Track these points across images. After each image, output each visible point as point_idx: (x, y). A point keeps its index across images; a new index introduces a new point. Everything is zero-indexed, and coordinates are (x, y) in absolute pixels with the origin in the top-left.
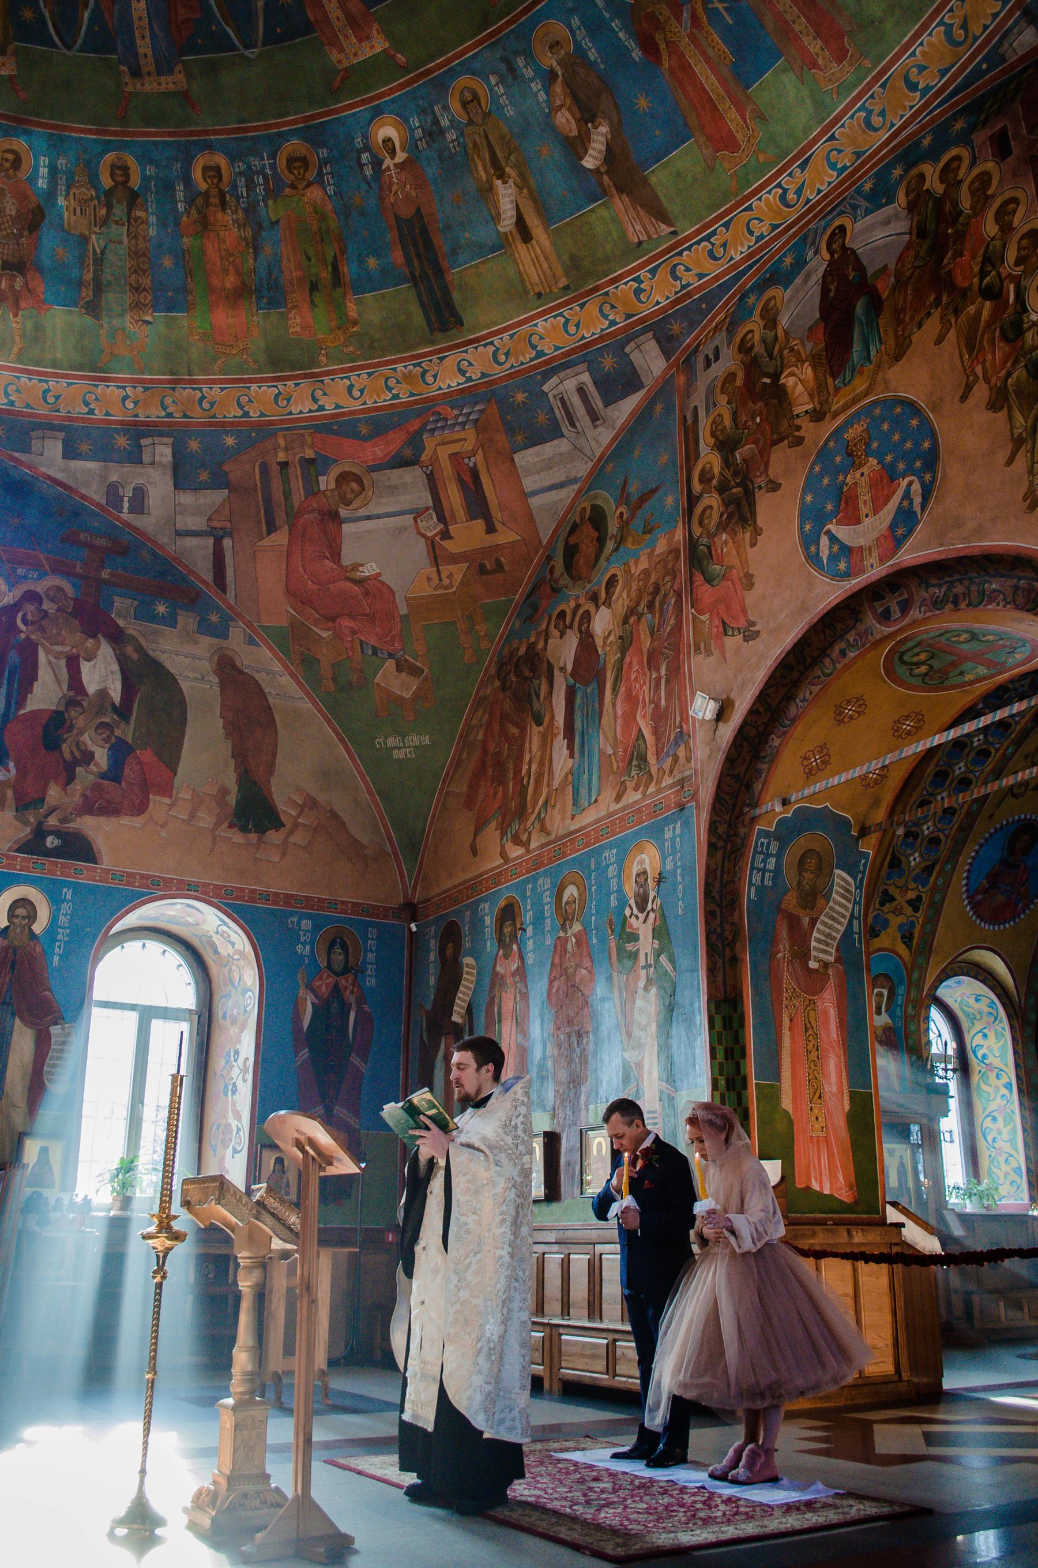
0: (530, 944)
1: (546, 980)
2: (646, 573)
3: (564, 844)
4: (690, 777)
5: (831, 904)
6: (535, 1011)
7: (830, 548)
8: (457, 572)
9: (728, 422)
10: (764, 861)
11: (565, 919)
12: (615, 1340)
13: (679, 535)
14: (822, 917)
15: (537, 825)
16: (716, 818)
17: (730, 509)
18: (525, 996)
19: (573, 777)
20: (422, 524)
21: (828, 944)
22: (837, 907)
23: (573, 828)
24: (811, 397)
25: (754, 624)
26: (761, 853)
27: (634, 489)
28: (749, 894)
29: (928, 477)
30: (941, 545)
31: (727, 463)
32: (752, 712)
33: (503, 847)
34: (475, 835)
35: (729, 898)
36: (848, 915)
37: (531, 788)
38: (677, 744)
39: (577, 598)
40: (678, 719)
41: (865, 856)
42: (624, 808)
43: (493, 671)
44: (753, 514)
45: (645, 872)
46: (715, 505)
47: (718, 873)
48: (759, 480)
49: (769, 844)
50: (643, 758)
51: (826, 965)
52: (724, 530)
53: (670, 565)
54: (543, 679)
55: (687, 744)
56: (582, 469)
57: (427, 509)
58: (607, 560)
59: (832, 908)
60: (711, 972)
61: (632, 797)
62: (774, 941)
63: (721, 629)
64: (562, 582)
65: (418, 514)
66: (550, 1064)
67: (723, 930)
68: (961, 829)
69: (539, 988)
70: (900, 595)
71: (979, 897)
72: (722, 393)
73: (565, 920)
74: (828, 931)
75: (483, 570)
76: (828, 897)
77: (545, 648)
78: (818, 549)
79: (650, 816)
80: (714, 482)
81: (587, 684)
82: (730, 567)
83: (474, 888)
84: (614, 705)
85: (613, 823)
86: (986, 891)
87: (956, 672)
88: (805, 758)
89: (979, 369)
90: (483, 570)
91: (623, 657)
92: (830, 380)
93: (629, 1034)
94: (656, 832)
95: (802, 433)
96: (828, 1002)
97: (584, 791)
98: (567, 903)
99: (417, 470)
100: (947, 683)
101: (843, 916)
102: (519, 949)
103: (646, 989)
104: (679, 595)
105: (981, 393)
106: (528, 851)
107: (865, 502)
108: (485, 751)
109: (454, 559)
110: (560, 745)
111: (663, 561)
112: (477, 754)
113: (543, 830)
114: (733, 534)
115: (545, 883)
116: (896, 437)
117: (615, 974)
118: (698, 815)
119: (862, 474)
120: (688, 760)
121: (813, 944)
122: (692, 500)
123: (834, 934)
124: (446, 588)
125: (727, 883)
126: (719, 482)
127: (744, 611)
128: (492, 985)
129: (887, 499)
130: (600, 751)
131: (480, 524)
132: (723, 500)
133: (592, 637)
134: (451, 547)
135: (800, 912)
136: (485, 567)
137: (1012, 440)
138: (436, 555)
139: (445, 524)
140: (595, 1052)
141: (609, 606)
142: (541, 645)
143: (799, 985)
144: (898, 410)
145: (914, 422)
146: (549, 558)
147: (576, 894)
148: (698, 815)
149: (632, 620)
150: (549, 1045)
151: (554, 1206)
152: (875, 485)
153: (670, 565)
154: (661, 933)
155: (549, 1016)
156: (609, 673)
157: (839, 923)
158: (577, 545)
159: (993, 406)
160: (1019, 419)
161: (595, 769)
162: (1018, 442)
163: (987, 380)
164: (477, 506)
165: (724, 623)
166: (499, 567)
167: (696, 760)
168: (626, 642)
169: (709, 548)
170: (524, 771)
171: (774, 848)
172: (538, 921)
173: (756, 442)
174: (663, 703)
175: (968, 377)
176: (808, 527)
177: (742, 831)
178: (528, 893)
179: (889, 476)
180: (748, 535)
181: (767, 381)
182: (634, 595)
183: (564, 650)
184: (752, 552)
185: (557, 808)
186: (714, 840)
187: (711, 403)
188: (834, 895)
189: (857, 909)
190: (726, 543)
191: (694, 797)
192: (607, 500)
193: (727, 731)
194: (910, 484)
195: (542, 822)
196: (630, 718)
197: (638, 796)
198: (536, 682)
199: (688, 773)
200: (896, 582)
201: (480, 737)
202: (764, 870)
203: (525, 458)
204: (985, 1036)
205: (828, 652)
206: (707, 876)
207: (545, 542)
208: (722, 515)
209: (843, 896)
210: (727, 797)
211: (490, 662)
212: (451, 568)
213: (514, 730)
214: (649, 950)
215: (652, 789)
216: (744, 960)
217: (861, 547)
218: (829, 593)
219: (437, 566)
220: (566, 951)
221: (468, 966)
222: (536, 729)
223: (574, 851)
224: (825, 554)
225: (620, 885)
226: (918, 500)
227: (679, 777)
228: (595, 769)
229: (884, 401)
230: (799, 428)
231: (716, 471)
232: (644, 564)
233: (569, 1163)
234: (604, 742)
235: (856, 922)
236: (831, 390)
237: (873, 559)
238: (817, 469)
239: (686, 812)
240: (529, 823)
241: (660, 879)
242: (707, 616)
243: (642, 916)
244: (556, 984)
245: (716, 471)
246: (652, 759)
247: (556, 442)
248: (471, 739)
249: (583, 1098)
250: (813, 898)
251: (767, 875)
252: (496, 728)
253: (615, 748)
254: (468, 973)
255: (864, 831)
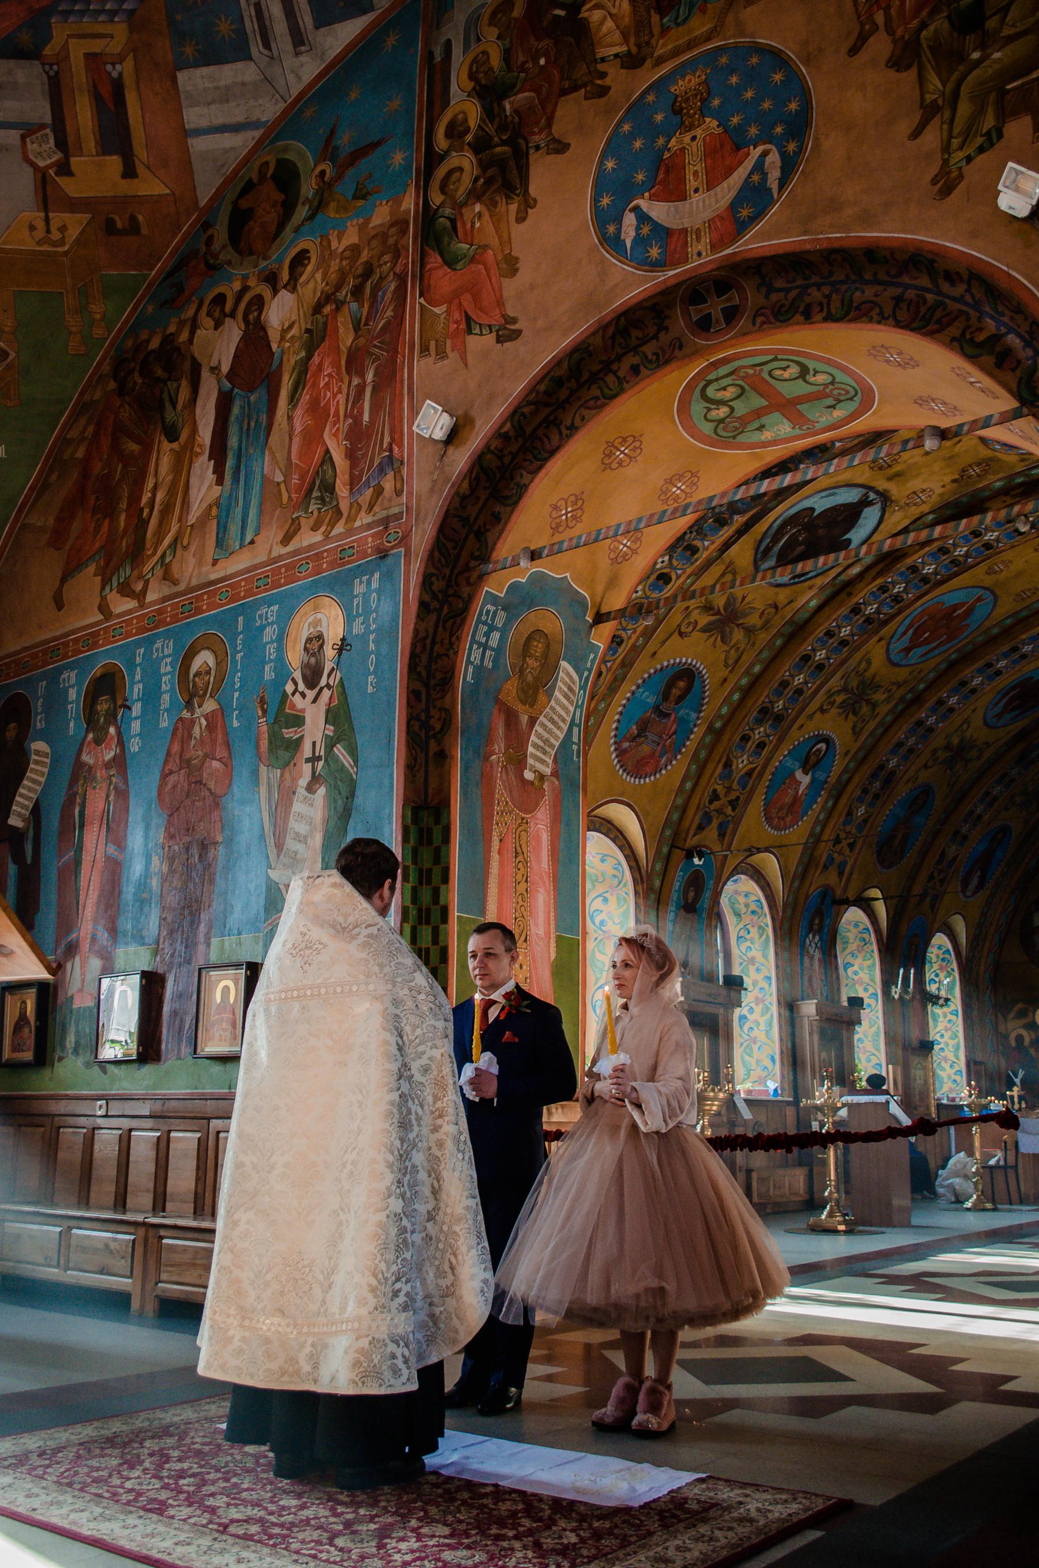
0: (136, 726)
1: (157, 776)
2: (355, 250)
3: (199, 598)
4: (398, 516)
5: (553, 703)
6: (136, 813)
7: (638, 229)
8: (75, 224)
9: (496, 61)
10: (487, 635)
11: (192, 696)
12: (70, 1228)
13: (409, 203)
14: (542, 718)
15: (159, 572)
16: (433, 570)
17: (490, 173)
18: (123, 795)
19: (220, 512)
20: (32, 147)
21: (545, 753)
22: (558, 708)
23: (213, 577)
24: (625, 35)
25: (514, 320)
26: (485, 623)
27: (345, 141)
28: (465, 675)
29: (792, 147)
30: (805, 233)
31: (489, 113)
32: (499, 435)
33: (103, 598)
34: (63, 580)
35: (439, 675)
36: (569, 719)
37: (153, 522)
38: (381, 470)
39: (245, 278)
40: (387, 440)
41: (594, 649)
42: (295, 553)
43: (106, 368)
44: (525, 180)
45: (320, 637)
46: (466, 165)
47: (428, 642)
48: (536, 138)
49: (495, 613)
50: (329, 488)
51: (542, 777)
52: (479, 199)
53: (391, 241)
54: (184, 383)
55: (398, 472)
56: (269, 110)
57: (43, 126)
58: (297, 230)
59: (553, 709)
60: (411, 769)
61: (308, 538)
62: (490, 740)
63: (463, 326)
64: (223, 257)
65: (29, 131)
66: (155, 883)
67: (429, 717)
68: (623, 664)
69: (145, 784)
70: (730, 299)
71: (626, 745)
72: (490, 24)
73: (191, 693)
74: (546, 735)
75: (110, 228)
76: (550, 695)
77: (191, 340)
78: (619, 230)
79: (333, 565)
80: (469, 138)
81: (251, 390)
82: (485, 247)
83: (56, 651)
84: (290, 418)
85: (276, 572)
86: (634, 739)
87: (756, 424)
88: (556, 508)
89: (879, 18)
90: (110, 228)
91: (309, 357)
92: (655, 18)
93: (279, 847)
94: (340, 587)
95: (608, 81)
96: (541, 823)
97: (234, 529)
98: (198, 674)
99: (35, 68)
100: (740, 439)
101: (564, 720)
102: (119, 733)
103: (310, 789)
104: (402, 279)
105: (880, 46)
106: (142, 605)
107: (696, 173)
108: (85, 474)
109: (74, 205)
110: (203, 470)
111: (383, 236)
112: (75, 475)
113: (167, 576)
114: (492, 204)
115: (166, 650)
116: (749, 94)
117: (263, 769)
118: (408, 564)
119: (694, 138)
120: (398, 493)
121: (530, 749)
122: (432, 159)
123: (552, 740)
124: (55, 244)
125: (439, 656)
126: (476, 137)
127: (500, 303)
128: (74, 780)
129: (729, 172)
130: (263, 476)
131: (114, 162)
132: (480, 162)
133: (264, 329)
134: (70, 187)
135: (519, 707)
136: (114, 222)
137: (922, 106)
138: (47, 195)
139: (67, 156)
140: (227, 869)
141: (293, 290)
142: (184, 336)
143: (512, 797)
144: (754, 60)
145: (778, 77)
146: (206, 225)
147: (211, 662)
148: (408, 564)
149: (327, 309)
150: (156, 861)
151: (148, 1069)
152: (712, 152)
153: (391, 241)
154: (339, 716)
155: (159, 820)
156: (286, 377)
157: (559, 728)
158: (251, 210)
159: (897, 63)
160: (934, 81)
161: (254, 502)
162: (929, 112)
163: (890, 30)
164: (115, 137)
165: (468, 319)
166: (133, 227)
167: (410, 494)
168: (315, 338)
169: (453, 221)
170: (144, 500)
171: (500, 620)
172: (151, 697)
173: (537, 90)
174: (366, 417)
175: (862, 25)
176: (605, 201)
177: (465, 591)
178: (138, 660)
179: (729, 147)
180: (513, 207)
181: (561, 13)
182: (333, 277)
183: (221, 345)
184: (518, 231)
185: (192, 548)
186: (427, 598)
187: (472, 32)
188: (557, 693)
189: (578, 714)
190: (480, 215)
191: (404, 540)
192: (302, 154)
193: (461, 459)
194: (765, 154)
195: (167, 569)
196: (313, 437)
197: (318, 537)
198: (172, 385)
199: (395, 510)
200: (724, 280)
201: (80, 454)
202: (485, 647)
203: (193, 80)
204: (606, 900)
205: (614, 367)
206: (414, 645)
207: (202, 203)
208: (476, 180)
209: (566, 696)
210: (449, 545)
211: (107, 353)
212: (66, 216)
213: (133, 447)
214: (319, 738)
215: (339, 529)
216: (453, 757)
217: (684, 231)
218: (630, 285)
219: (46, 210)
220: (190, 736)
221: (38, 753)
222: (166, 446)
223: (212, 606)
224: (629, 234)
225: (281, 650)
226: (774, 175)
227: (384, 514)
228: (254, 502)
229: (736, 47)
230: (603, 75)
231: (473, 123)
232: (352, 237)
233: (175, 1013)
234: (269, 466)
235: (575, 730)
236: (656, 30)
237: (703, 245)
238: (626, 128)
239: (390, 560)
240: (147, 568)
241: (343, 646)
242: (444, 308)
243: (311, 694)
244: (172, 779)
245: (473, 123)
246: (342, 490)
247: (239, 65)
248: (66, 456)
249: (202, 928)
250: (536, 688)
251: (488, 653)
252: (106, 443)
253: (287, 476)
254: (37, 762)
255: (600, 618)
